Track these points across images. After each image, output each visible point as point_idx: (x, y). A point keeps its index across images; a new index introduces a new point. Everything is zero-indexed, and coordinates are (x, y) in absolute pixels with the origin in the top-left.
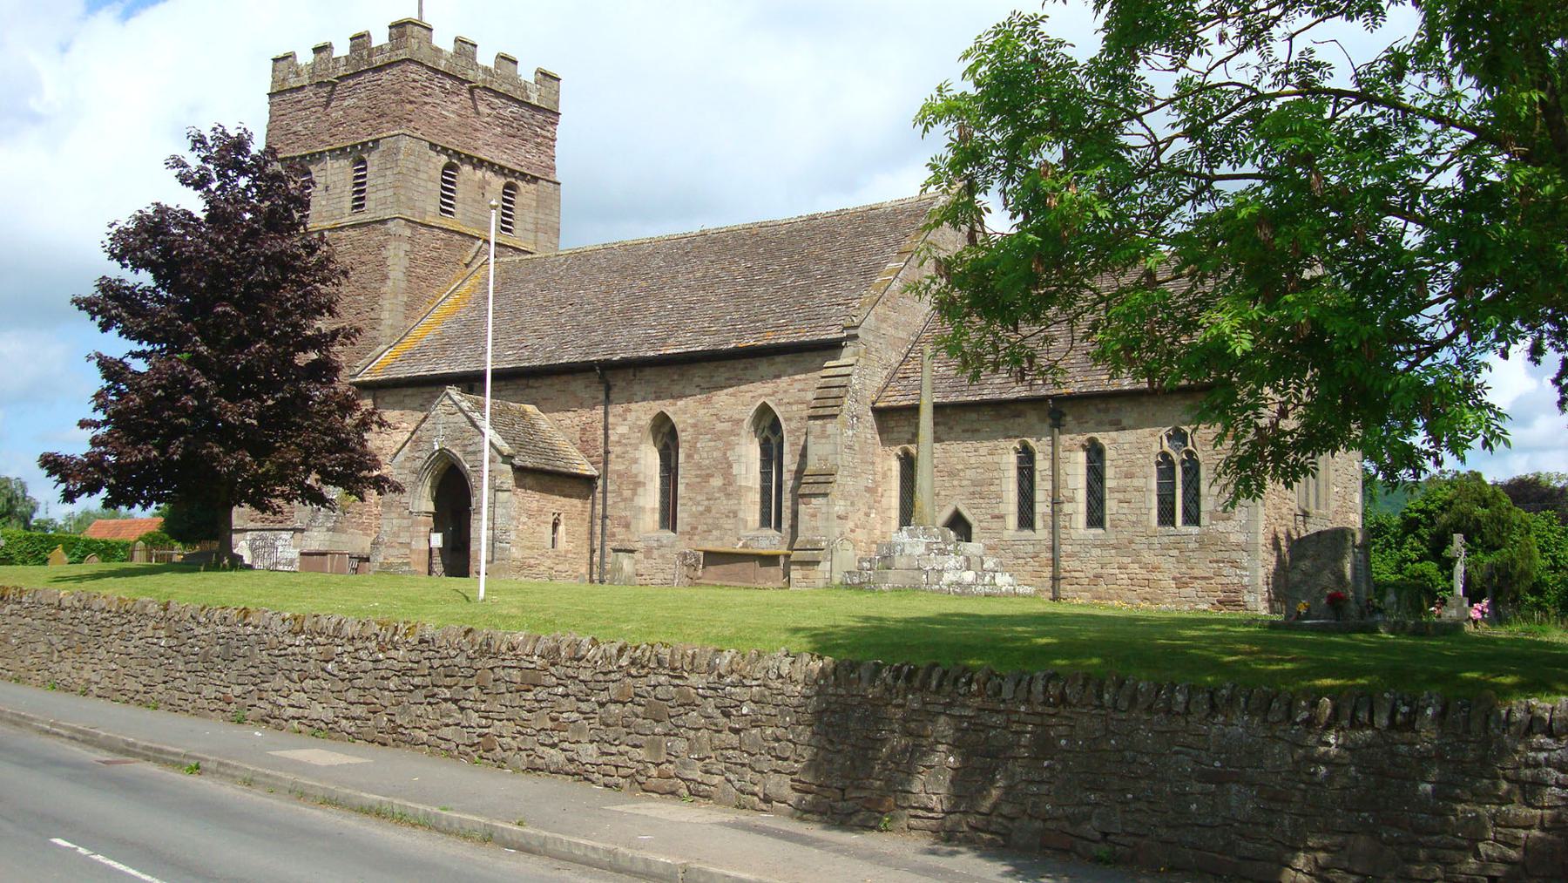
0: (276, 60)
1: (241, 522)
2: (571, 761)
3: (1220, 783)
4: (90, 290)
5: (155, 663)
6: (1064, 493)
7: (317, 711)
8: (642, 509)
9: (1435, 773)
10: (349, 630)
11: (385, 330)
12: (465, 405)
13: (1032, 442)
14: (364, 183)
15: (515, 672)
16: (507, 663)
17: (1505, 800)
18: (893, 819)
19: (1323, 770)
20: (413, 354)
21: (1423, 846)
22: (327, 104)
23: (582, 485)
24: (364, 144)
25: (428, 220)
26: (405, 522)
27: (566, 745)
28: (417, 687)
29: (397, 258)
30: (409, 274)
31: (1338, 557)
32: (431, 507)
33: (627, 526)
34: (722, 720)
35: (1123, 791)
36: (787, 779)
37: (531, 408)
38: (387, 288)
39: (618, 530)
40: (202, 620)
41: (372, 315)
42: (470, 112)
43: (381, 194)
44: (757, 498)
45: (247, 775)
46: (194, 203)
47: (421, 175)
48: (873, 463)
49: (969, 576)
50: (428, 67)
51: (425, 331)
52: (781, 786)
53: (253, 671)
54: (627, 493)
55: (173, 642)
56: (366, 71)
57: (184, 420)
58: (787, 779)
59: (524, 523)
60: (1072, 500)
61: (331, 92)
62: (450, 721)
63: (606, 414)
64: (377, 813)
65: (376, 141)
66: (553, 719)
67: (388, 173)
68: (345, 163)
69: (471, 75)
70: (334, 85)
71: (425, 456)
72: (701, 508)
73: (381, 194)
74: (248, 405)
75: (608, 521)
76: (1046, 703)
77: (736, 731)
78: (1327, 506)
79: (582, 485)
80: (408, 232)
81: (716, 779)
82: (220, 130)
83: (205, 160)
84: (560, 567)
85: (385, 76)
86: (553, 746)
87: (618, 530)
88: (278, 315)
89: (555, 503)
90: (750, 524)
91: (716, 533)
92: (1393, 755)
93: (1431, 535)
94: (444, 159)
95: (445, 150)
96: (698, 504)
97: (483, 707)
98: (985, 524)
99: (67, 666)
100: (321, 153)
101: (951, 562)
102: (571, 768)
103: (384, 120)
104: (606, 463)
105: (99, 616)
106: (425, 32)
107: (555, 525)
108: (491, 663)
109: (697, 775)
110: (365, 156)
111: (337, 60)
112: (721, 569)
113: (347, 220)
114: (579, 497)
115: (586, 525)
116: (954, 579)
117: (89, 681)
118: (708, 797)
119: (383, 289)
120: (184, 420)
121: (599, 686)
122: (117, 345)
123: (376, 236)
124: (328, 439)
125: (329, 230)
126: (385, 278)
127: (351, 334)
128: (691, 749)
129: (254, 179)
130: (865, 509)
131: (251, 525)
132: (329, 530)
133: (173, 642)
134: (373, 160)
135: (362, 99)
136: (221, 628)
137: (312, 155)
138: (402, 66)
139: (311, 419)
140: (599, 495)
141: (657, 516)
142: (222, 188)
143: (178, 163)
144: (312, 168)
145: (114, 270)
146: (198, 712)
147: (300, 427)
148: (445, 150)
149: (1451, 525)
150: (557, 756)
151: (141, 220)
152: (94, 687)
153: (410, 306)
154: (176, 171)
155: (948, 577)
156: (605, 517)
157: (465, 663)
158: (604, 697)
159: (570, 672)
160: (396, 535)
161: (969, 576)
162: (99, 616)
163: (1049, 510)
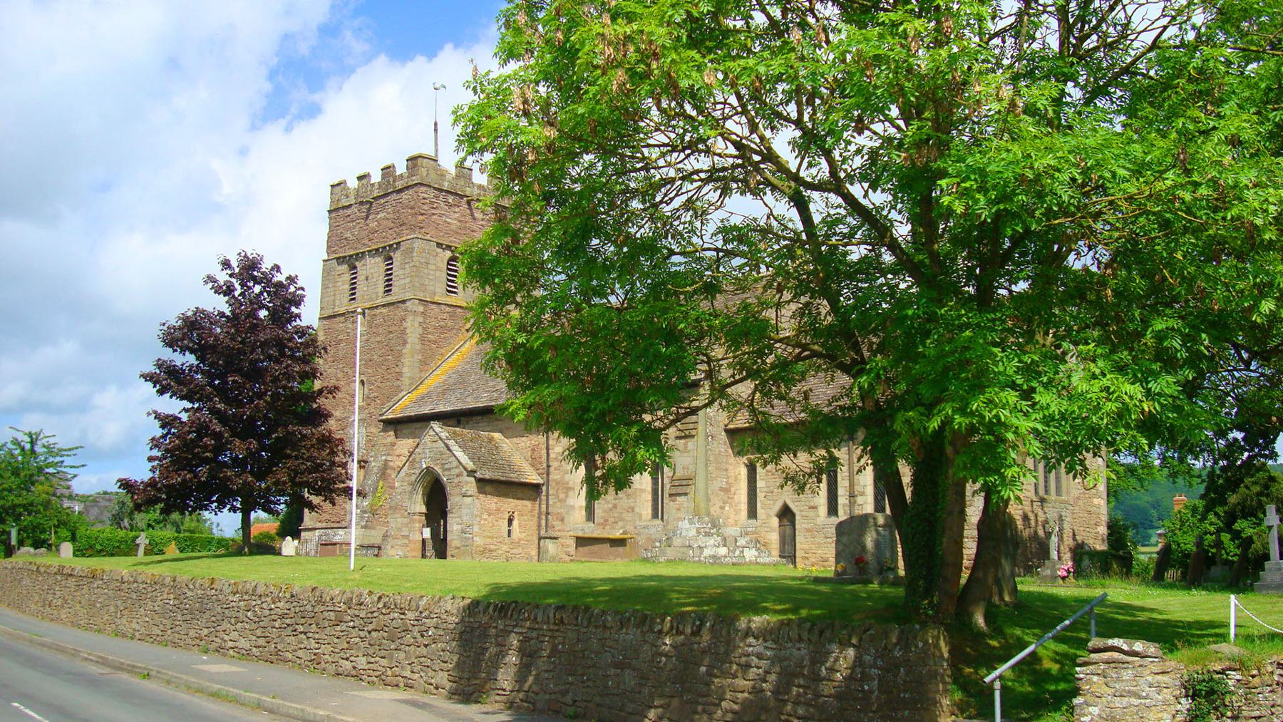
0: (333, 186)
1: (312, 523)
2: (354, 668)
3: (622, 669)
4: (151, 368)
5: (167, 615)
6: (857, 489)
7: (243, 643)
8: (572, 507)
9: (707, 661)
10: (260, 590)
11: (406, 381)
12: (444, 435)
13: (836, 453)
14: (391, 274)
15: (332, 613)
16: (329, 608)
17: (735, 676)
18: (488, 696)
19: (664, 659)
20: (423, 398)
21: (701, 704)
22: (367, 217)
23: (532, 491)
24: (391, 246)
25: (437, 299)
26: (406, 520)
27: (352, 658)
28: (288, 625)
29: (413, 328)
30: (422, 339)
31: (862, 534)
32: (423, 509)
33: (562, 520)
34: (420, 639)
35: (583, 675)
36: (446, 674)
37: (497, 435)
38: (407, 350)
39: (557, 523)
40: (191, 587)
41: (397, 370)
42: (468, 218)
43: (402, 282)
44: (649, 497)
45: (168, 678)
46: (220, 304)
47: (430, 267)
48: (727, 470)
49: (723, 551)
50: (435, 188)
51: (434, 380)
52: (443, 678)
53: (213, 619)
54: (562, 496)
55: (177, 602)
56: (392, 193)
57: (208, 454)
58: (446, 674)
59: (485, 520)
60: (862, 494)
61: (369, 209)
62: (302, 646)
63: (547, 438)
64: (215, 695)
65: (398, 244)
66: (348, 643)
67: (407, 266)
68: (379, 260)
69: (468, 191)
70: (371, 203)
71: (417, 472)
72: (610, 506)
73: (402, 282)
74: (251, 443)
75: (550, 517)
76: (555, 624)
77: (426, 646)
78: (1068, 493)
79: (532, 491)
80: (421, 309)
81: (416, 676)
82: (243, 254)
83: (231, 276)
84: (515, 551)
85: (404, 196)
86: (347, 659)
87: (557, 523)
88: (271, 381)
89: (510, 504)
90: (644, 517)
91: (620, 524)
92: (692, 650)
93: (1225, 512)
94: (448, 254)
95: (449, 247)
96: (609, 502)
97: (317, 636)
98: (804, 513)
99: (124, 621)
100: (363, 253)
101: (711, 541)
102: (354, 672)
103: (404, 228)
104: (548, 474)
105: (142, 586)
106: (432, 162)
107: (510, 521)
108: (322, 608)
109: (408, 674)
110: (392, 254)
111: (373, 185)
112: (586, 549)
113: (380, 301)
114: (529, 499)
115: (535, 519)
116: (711, 553)
117: (134, 630)
118: (411, 687)
119: (404, 351)
120: (208, 454)
121: (369, 621)
122: (174, 406)
123: (399, 312)
124: (309, 464)
125: (369, 309)
126: (405, 343)
127: (333, 390)
128: (406, 658)
129: (264, 287)
130: (721, 504)
131: (319, 525)
132: (362, 527)
133: (177, 602)
134: (397, 256)
135: (388, 213)
136: (199, 592)
137: (357, 254)
138: (416, 189)
139: (299, 451)
140: (544, 498)
141: (584, 513)
142: (242, 294)
143: (210, 279)
144: (357, 263)
145: (168, 354)
146: (187, 647)
147: (289, 457)
148: (449, 247)
149: (1239, 504)
150: (347, 665)
151: (186, 320)
152: (137, 634)
153: (424, 363)
154: (210, 285)
155: (707, 552)
156: (548, 513)
157: (310, 609)
158: (370, 627)
159: (357, 613)
160: (399, 529)
161: (723, 551)
162: (142, 586)
163: (847, 502)
